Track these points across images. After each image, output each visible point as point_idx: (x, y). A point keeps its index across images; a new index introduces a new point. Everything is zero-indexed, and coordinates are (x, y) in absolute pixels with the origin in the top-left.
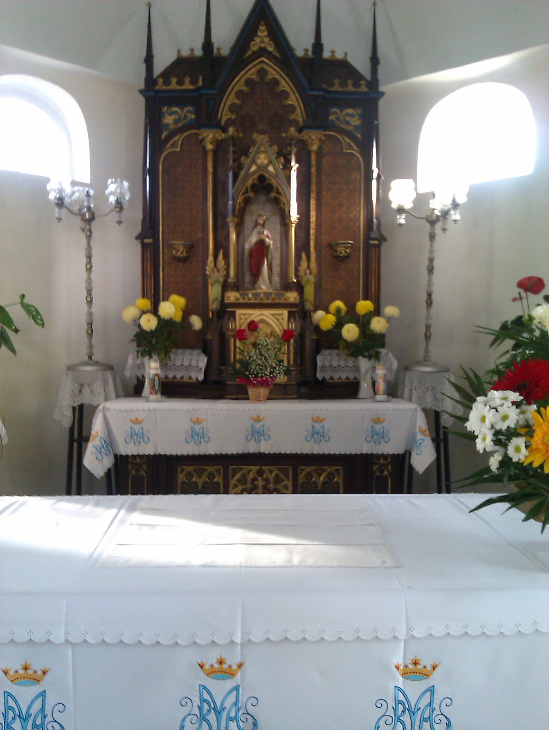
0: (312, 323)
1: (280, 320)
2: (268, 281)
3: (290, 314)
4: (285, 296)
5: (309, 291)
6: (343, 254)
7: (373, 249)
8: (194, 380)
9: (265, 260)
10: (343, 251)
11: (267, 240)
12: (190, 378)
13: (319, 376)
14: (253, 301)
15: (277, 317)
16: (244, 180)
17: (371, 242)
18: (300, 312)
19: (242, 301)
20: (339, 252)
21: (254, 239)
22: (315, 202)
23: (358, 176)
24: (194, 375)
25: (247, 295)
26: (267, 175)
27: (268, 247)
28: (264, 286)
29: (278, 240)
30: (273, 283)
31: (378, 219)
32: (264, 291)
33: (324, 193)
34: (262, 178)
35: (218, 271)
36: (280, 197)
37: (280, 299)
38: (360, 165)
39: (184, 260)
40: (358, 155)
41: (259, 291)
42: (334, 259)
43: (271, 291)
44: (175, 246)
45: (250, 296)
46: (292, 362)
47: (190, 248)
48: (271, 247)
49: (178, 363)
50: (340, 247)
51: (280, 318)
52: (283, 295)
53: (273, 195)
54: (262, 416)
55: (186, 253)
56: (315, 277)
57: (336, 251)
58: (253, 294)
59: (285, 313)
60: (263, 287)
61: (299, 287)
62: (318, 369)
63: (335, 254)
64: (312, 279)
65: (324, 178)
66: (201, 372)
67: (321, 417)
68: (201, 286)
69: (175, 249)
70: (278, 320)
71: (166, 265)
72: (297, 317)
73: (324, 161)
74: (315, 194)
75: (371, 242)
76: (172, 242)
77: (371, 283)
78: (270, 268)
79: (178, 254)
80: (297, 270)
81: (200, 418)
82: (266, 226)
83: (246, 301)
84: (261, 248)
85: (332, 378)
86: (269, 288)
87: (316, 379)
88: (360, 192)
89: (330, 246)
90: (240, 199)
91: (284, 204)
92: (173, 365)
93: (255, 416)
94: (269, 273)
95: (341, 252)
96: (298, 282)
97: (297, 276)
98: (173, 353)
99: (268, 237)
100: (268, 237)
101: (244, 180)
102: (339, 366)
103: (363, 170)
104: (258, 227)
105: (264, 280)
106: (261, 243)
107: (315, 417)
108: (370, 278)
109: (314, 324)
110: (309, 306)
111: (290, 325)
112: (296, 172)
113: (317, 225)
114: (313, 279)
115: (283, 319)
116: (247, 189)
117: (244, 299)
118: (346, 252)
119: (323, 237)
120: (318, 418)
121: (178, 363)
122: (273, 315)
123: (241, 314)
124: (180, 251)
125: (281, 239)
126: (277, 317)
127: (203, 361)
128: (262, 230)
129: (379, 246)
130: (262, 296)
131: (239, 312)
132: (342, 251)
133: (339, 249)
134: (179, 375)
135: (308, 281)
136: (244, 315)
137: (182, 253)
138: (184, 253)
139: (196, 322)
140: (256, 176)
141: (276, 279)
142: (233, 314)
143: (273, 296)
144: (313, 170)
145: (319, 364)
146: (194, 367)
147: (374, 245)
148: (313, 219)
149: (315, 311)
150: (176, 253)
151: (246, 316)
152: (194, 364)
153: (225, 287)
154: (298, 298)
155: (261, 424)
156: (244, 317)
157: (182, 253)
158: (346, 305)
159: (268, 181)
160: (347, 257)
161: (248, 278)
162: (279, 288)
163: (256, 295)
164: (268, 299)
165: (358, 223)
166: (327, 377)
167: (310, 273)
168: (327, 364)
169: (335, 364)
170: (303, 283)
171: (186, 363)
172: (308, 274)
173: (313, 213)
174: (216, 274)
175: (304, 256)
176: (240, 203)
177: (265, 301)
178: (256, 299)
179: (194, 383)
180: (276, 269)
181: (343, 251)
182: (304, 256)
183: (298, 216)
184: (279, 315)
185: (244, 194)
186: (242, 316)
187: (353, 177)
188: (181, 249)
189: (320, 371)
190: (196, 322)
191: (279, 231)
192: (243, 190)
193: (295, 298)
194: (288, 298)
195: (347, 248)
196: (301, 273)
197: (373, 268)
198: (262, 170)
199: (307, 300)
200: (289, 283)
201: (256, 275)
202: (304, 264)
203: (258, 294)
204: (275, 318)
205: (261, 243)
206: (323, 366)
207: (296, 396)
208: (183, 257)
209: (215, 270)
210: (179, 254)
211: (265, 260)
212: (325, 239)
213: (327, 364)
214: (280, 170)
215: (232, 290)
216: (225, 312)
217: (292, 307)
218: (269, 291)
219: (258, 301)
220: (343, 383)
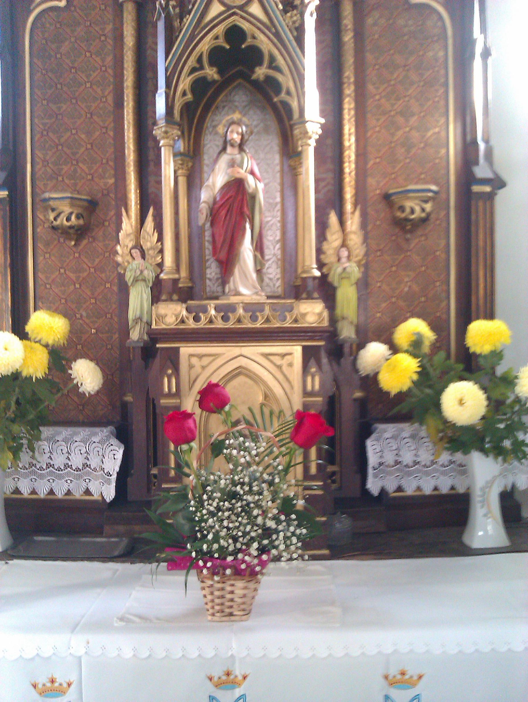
0: (356, 370)
1: (284, 368)
2: (254, 275)
3: (308, 354)
4: (295, 312)
5: (347, 295)
6: (418, 214)
7: (481, 204)
8: (96, 497)
9: (248, 226)
10: (417, 209)
11: (250, 180)
12: (87, 492)
13: (373, 486)
14: (219, 324)
15: (277, 360)
16: (193, 40)
17: (476, 188)
18: (330, 349)
19: (191, 324)
20: (408, 210)
21: (217, 179)
22: (353, 105)
23: (441, 54)
24: (95, 487)
25: (205, 310)
26: (245, 26)
27: (253, 197)
28: (246, 286)
29: (276, 186)
30: (266, 280)
31: (487, 141)
32: (247, 300)
33: (370, 87)
34: (235, 34)
35: (143, 257)
36: (280, 78)
37: (284, 319)
38: (444, 28)
39: (80, 233)
40: (440, 9)
41: (234, 299)
42: (395, 225)
43: (262, 298)
44: (51, 203)
45: (213, 312)
46: (313, 470)
47: (91, 207)
48: (261, 196)
49: (59, 461)
50: (408, 198)
51: (284, 362)
52: (291, 309)
53: (261, 72)
54: (238, 672)
55: (78, 217)
56: (359, 263)
57: (402, 209)
58: (217, 309)
59: (296, 350)
60: (243, 290)
61: (326, 290)
62: (370, 471)
63: (399, 214)
64: (355, 271)
65: (369, 57)
66: (109, 482)
67: (412, 671)
68: (115, 288)
69: (53, 210)
70: (279, 367)
71: (40, 245)
72: (325, 360)
73: (370, 21)
74: (352, 87)
75: (476, 188)
76: (47, 195)
77: (477, 275)
78: (259, 247)
79: (58, 222)
80: (319, 251)
81: (61, 679)
82: (246, 148)
83: (202, 324)
84: (237, 200)
85: (400, 489)
86: (256, 293)
87: (366, 493)
88: (446, 84)
89: (387, 198)
90: (185, 83)
91: (288, 93)
92: (49, 465)
93: (218, 672)
94: (255, 257)
95: (412, 212)
96: (324, 277)
97: (321, 265)
98: (48, 439)
99: (252, 173)
100: (252, 173)
101: (192, 37)
102: (416, 463)
103: (450, 42)
104: (229, 149)
105: (244, 274)
106: (236, 187)
107: (393, 671)
108: (473, 268)
109: (363, 373)
110: (347, 332)
111: (309, 379)
112: (315, 15)
113: (358, 155)
114: (356, 269)
115: (291, 365)
116: (199, 60)
117: (197, 319)
118: (423, 210)
119: (371, 181)
120: (403, 674)
121: (59, 461)
122: (266, 356)
123: (191, 355)
124: (65, 212)
125: (282, 184)
126: (277, 360)
127: (113, 457)
128: (238, 157)
129: (490, 197)
130: (241, 311)
131: (186, 350)
132: (414, 207)
133: (408, 204)
134: (60, 490)
135: (345, 275)
136: (200, 357)
137: (68, 219)
138: (73, 218)
139: (87, 375)
140: (220, 29)
141: (273, 271)
142: (173, 359)
143: (267, 310)
144: (348, 37)
145: (372, 459)
146: (95, 470)
147: (482, 194)
148: (350, 141)
149: (361, 345)
150: (55, 219)
151: (206, 361)
152: (94, 462)
153: (158, 291)
154: (326, 314)
155: (238, 692)
156: (203, 363)
157: (68, 219)
158: (433, 327)
159: (249, 41)
160: (424, 221)
161: (212, 271)
162: (280, 291)
163: (226, 311)
164: (254, 319)
165: (443, 151)
166: (391, 486)
167: (349, 258)
168: (389, 458)
169: (407, 458)
170: (334, 278)
171: (77, 461)
172: (344, 260)
173: (349, 129)
174: (139, 261)
175: (333, 218)
176: (184, 94)
177: (248, 325)
178: (225, 319)
179: (95, 502)
180: (273, 250)
181: (417, 209)
182: (333, 218)
183: (323, 121)
184: (283, 356)
185: (193, 70)
186: (194, 360)
187: (430, 54)
188: (67, 210)
189: (375, 476)
190: (87, 375)
191: (278, 168)
192: (192, 62)
193: (320, 314)
194: (304, 315)
195: (426, 202)
196: (329, 257)
197: (481, 243)
198: (234, 14)
199: (343, 318)
200: (304, 279)
201: (227, 263)
202: (334, 238)
203: (232, 308)
204: (272, 362)
205: (236, 187)
206: (381, 464)
207: (326, 552)
208: (71, 227)
209: (136, 253)
210: (62, 221)
211: (248, 226)
212: (376, 185)
213: (389, 458)
214: (278, 13)
215: (170, 299)
216: (156, 351)
217: (312, 339)
218: (256, 299)
219: (230, 325)
220: (424, 497)
